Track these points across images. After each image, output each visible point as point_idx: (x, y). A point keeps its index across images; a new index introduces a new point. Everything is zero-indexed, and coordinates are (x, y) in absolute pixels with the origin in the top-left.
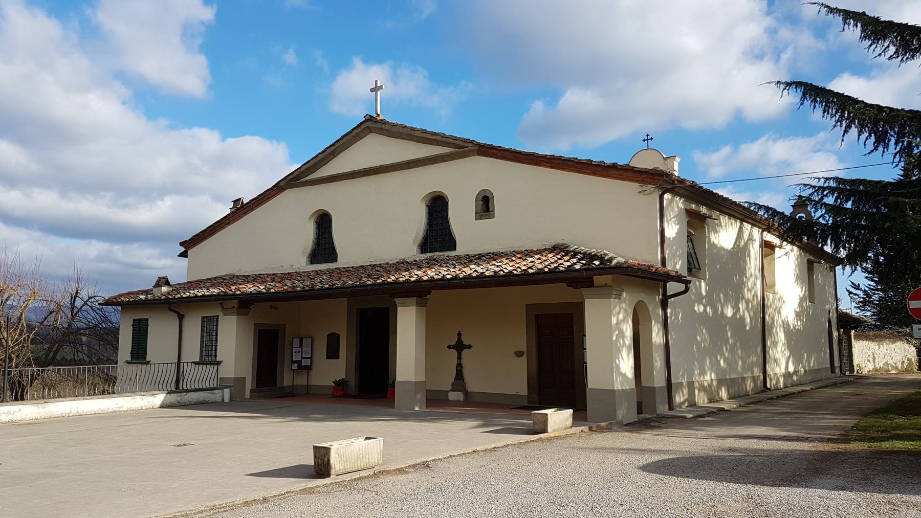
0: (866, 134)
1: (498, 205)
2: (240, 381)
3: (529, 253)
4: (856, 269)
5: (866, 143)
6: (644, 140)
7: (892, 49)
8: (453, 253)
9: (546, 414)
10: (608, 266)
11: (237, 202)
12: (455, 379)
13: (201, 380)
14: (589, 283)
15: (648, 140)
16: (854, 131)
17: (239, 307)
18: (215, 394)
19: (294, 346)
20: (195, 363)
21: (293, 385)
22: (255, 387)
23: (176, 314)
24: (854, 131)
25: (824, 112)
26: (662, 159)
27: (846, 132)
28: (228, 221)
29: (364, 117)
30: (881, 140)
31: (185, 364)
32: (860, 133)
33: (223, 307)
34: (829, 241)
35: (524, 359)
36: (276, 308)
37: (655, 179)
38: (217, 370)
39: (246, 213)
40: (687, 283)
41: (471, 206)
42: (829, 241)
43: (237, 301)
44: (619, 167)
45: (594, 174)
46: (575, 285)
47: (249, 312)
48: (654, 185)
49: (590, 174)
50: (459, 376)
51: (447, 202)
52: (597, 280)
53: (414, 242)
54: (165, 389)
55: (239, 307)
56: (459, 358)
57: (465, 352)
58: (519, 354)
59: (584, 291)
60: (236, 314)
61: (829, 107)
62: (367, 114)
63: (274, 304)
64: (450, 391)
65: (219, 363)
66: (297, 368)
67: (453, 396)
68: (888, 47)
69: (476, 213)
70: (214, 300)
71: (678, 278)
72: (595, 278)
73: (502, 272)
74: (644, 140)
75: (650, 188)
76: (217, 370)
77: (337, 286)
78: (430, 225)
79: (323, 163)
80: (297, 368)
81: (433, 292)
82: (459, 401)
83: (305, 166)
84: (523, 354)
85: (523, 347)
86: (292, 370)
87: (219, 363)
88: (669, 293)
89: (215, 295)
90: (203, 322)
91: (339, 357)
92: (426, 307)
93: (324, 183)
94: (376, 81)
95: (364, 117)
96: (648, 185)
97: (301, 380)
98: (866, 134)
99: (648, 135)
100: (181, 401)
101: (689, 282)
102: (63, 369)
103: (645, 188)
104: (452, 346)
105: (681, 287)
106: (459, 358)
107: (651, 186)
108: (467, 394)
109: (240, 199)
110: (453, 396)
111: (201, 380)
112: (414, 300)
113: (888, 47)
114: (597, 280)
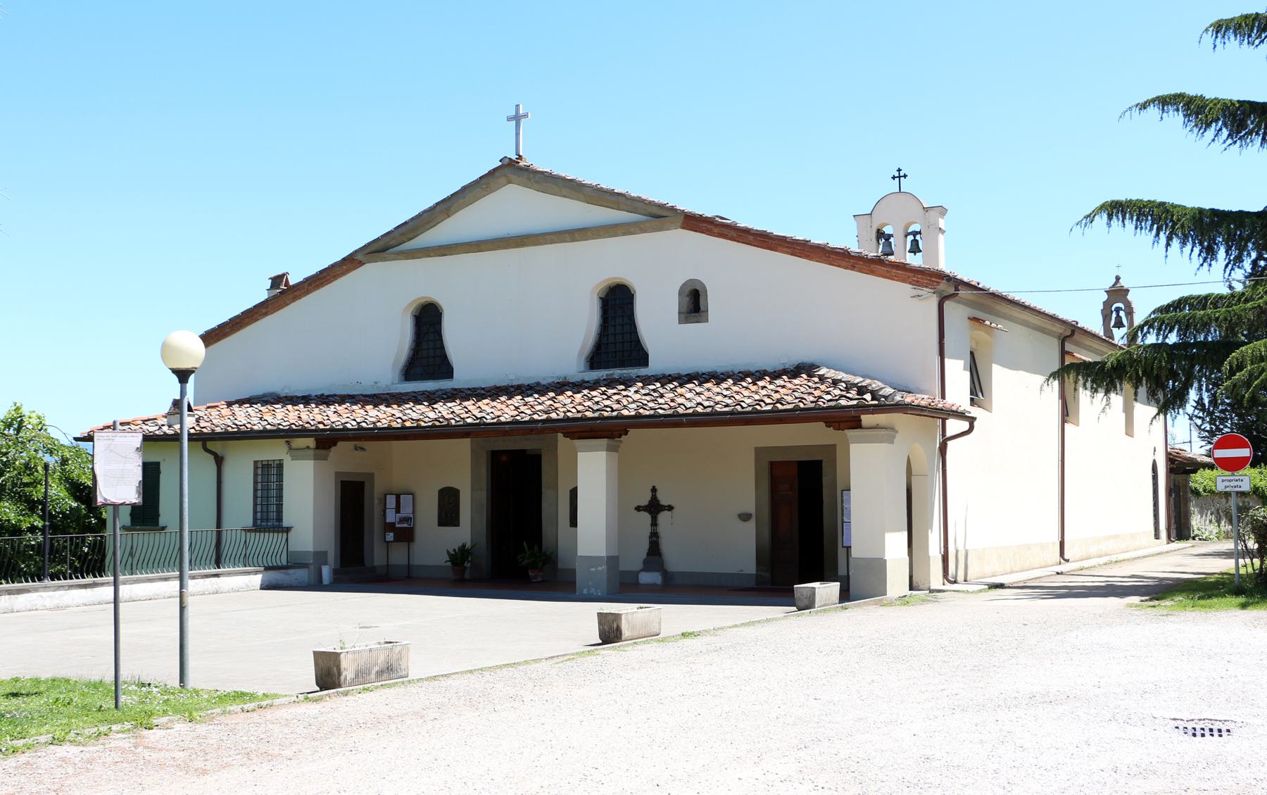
0: (1189, 246)
1: (713, 303)
2: (320, 557)
3: (758, 376)
4: (1178, 413)
5: (1192, 257)
6: (894, 178)
7: (1225, 132)
8: (643, 371)
9: (814, 588)
10: (883, 403)
11: (278, 280)
12: (648, 554)
13: (256, 556)
14: (856, 424)
15: (899, 177)
16: (1176, 243)
17: (317, 448)
18: (289, 574)
19: (388, 507)
20: (249, 531)
21: (388, 565)
22: (338, 567)
23: (213, 457)
24: (1176, 243)
25: (1136, 228)
26: (922, 210)
27: (1168, 245)
28: (264, 311)
29: (501, 161)
30: (1209, 253)
31: (199, 533)
32: (1184, 243)
33: (290, 448)
34: (1144, 382)
35: (752, 525)
36: (362, 449)
37: (934, 281)
38: (287, 539)
39: (295, 298)
40: (972, 420)
41: (672, 304)
42: (1144, 382)
43: (313, 439)
44: (887, 262)
45: (853, 268)
46: (837, 425)
47: (328, 455)
48: (931, 288)
49: (846, 268)
50: (654, 548)
51: (633, 295)
52: (866, 419)
53: (580, 353)
54: (261, 564)
55: (317, 448)
56: (654, 523)
57: (663, 517)
58: (745, 517)
59: (850, 433)
60: (313, 458)
61: (1141, 222)
62: (506, 157)
63: (359, 443)
64: (642, 570)
65: (288, 530)
66: (392, 539)
67: (647, 578)
68: (1221, 129)
69: (679, 313)
70: (282, 437)
71: (960, 415)
72: (864, 417)
73: (739, 407)
74: (894, 178)
75: (925, 292)
76: (287, 539)
77: (485, 420)
78: (604, 326)
79: (428, 226)
80: (392, 539)
81: (632, 432)
82: (655, 585)
83: (400, 230)
84: (751, 517)
85: (751, 508)
86: (385, 541)
87: (288, 530)
88: (949, 434)
89: (283, 430)
90: (256, 468)
91: (459, 523)
92: (617, 452)
93: (430, 256)
94: (517, 106)
95: (501, 161)
96: (924, 289)
97: (398, 556)
98: (1189, 246)
99: (899, 170)
100: (249, 584)
101: (974, 419)
102: (70, 537)
103: (920, 292)
104: (643, 507)
105: (965, 425)
106: (654, 523)
107: (927, 289)
108: (667, 576)
109: (283, 275)
110: (647, 578)
111: (256, 556)
112: (604, 442)
113: (1221, 129)
114: (866, 419)
